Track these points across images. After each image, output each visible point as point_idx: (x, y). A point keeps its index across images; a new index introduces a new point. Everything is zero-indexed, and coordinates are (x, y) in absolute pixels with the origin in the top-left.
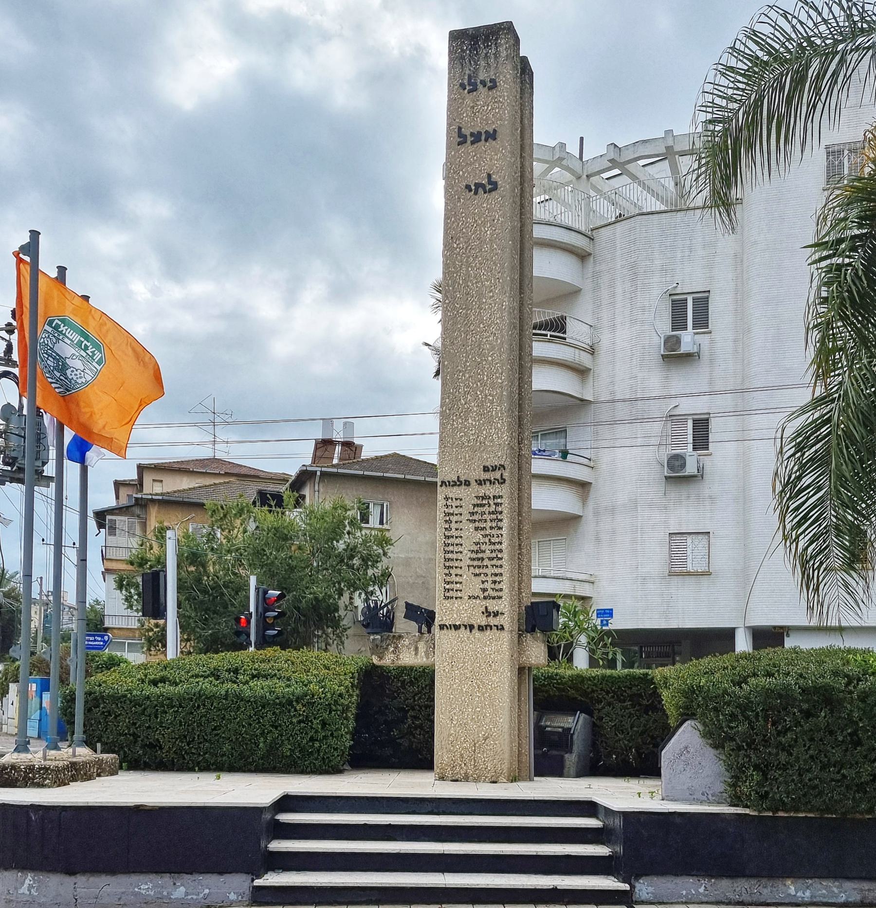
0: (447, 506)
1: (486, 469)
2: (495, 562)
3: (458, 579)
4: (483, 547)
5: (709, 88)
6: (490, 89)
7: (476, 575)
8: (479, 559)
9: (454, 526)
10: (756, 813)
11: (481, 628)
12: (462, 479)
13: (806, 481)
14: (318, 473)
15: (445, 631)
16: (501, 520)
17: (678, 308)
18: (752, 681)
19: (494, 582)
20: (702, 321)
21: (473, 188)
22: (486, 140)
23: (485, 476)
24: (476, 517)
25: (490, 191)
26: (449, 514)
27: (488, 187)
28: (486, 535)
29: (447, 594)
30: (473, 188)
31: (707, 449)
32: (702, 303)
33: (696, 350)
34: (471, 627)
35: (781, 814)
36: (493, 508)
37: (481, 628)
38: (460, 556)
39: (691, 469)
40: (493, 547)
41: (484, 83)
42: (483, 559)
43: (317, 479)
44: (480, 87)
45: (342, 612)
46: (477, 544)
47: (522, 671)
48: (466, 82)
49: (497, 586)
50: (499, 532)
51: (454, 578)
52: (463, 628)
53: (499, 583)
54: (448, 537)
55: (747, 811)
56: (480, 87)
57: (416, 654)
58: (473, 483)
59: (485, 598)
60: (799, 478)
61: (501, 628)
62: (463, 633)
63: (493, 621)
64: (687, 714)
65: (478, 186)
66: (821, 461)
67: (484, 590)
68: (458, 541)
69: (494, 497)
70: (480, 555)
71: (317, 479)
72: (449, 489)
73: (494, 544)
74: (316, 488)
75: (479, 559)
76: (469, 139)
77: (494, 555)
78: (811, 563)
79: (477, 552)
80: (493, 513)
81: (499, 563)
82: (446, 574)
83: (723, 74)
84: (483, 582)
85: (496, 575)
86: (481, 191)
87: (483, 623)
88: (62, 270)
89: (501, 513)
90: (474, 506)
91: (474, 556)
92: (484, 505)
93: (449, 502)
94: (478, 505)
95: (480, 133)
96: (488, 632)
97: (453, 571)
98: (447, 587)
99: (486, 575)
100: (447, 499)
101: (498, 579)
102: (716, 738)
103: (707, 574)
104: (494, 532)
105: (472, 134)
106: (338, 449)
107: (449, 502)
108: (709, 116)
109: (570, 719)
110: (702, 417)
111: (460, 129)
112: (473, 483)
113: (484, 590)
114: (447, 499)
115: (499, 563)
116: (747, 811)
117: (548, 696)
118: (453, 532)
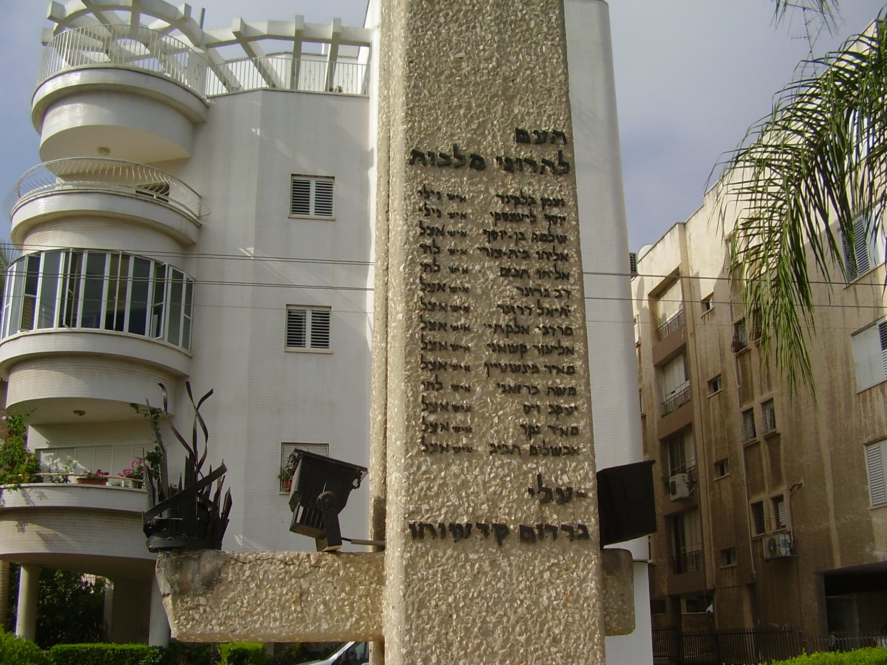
3: (457, 399)
4: (524, 320)
19: (557, 410)
46: (507, 309)
62: (478, 553)
67: (531, 431)
79: (508, 331)
97: (447, 377)
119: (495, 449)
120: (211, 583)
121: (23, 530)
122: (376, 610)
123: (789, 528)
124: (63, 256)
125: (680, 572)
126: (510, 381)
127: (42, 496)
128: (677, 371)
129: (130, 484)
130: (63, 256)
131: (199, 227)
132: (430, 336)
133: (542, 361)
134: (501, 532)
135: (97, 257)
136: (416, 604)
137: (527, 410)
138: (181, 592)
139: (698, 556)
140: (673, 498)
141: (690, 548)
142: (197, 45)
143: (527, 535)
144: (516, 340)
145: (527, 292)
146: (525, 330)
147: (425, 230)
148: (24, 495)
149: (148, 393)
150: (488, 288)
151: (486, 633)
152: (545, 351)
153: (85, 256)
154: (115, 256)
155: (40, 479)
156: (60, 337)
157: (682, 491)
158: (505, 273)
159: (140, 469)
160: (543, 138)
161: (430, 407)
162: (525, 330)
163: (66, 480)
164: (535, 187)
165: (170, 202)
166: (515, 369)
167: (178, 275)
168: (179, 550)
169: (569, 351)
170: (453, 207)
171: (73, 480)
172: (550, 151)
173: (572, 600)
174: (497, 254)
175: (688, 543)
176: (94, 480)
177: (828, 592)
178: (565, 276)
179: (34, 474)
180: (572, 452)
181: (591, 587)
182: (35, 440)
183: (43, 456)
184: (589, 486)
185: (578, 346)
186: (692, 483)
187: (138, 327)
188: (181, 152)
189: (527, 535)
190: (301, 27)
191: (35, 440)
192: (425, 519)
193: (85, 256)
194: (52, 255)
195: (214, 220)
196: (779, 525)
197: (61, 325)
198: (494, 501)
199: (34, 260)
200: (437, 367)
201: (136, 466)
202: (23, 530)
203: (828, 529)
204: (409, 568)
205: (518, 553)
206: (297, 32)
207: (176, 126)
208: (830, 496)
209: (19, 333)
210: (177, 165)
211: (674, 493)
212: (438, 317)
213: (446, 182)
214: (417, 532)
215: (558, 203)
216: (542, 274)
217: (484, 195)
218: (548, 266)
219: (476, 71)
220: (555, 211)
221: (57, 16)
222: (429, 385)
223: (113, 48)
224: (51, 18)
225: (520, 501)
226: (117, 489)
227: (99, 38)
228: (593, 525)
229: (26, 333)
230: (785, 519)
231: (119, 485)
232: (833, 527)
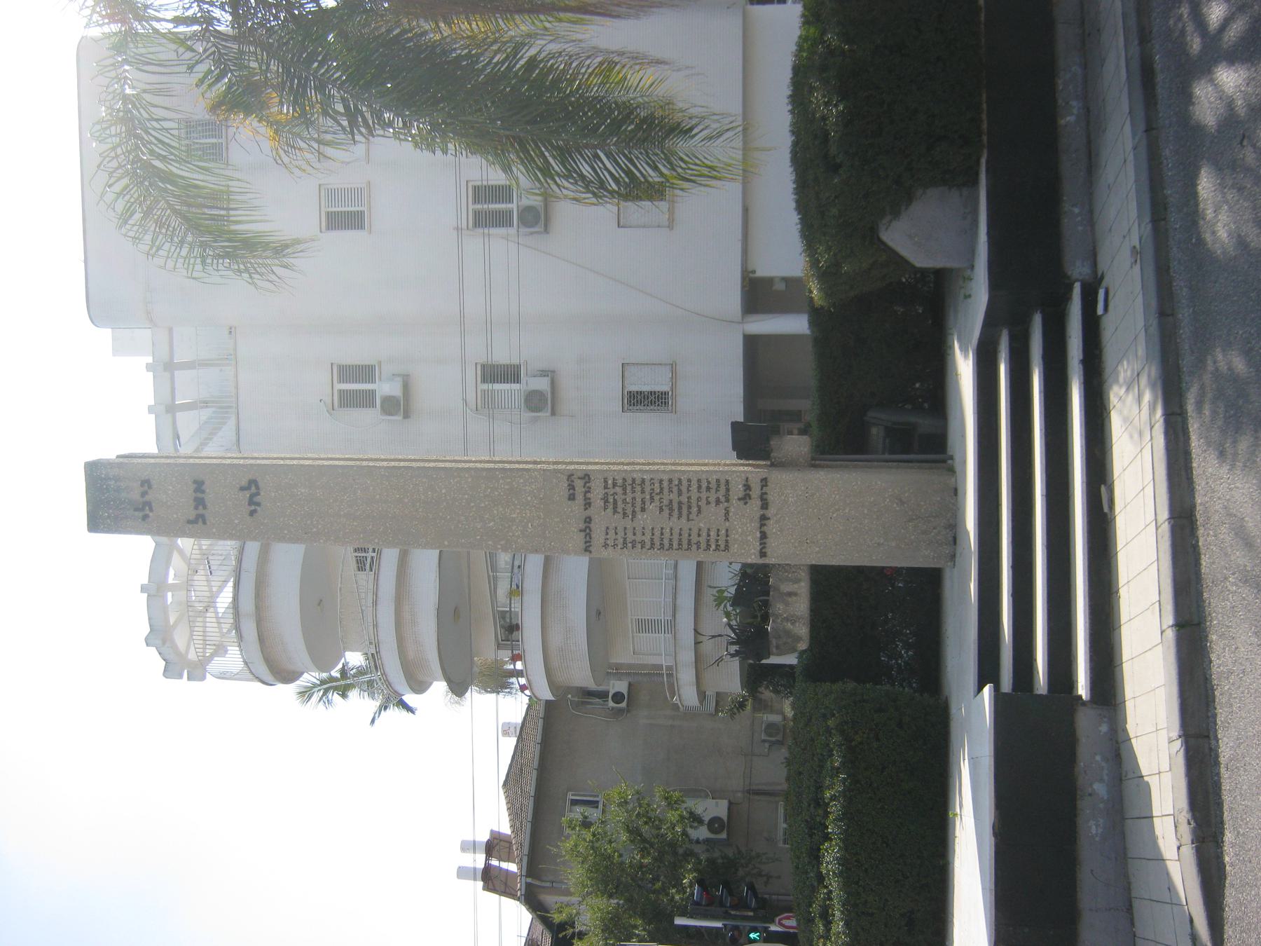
0: (615, 546)
1: (572, 498)
2: (684, 489)
3: (704, 534)
4: (666, 502)
5: (170, 264)
6: (150, 487)
7: (699, 511)
8: (680, 508)
9: (639, 538)
10: (985, 151)
11: (765, 506)
12: (582, 526)
13: (586, 170)
14: (529, 880)
15: (769, 551)
16: (634, 480)
17: (349, 400)
18: (833, 150)
19: (708, 489)
20: (366, 372)
21: (253, 508)
22: (203, 492)
23: (580, 498)
24: (629, 512)
25: (257, 488)
26: (625, 543)
27: (253, 489)
28: (652, 498)
29: (722, 547)
30: (253, 508)
31: (519, 367)
32: (348, 372)
33: (399, 379)
34: (764, 518)
35: (985, 126)
36: (618, 490)
37: (765, 506)
38: (676, 531)
39: (542, 384)
40: (666, 491)
41: (144, 494)
42: (680, 503)
43: (537, 883)
44: (147, 498)
45: (717, 854)
46: (661, 509)
47: (813, 464)
48: (141, 514)
49: (713, 485)
50: (647, 483)
51: (703, 540)
52: (765, 528)
53: (709, 483)
54: (653, 544)
55: (983, 161)
56: (147, 498)
57: (795, 594)
58: (588, 513)
59: (727, 501)
60: (582, 177)
61: (764, 482)
62: (771, 528)
63: (756, 492)
64: (871, 236)
65: (251, 502)
66: (564, 154)
67: (718, 502)
68: (657, 533)
69: (606, 487)
70: (675, 506)
71: (537, 883)
72: (594, 542)
73: (662, 489)
74: (548, 884)
75: (680, 508)
76: (201, 511)
77: (675, 489)
78: (679, 170)
79: (671, 510)
80: (625, 489)
81: (685, 483)
82: (698, 548)
83: (159, 249)
84: (708, 503)
85: (699, 487)
86: (257, 499)
87: (759, 503)
88: (409, 709)
89: (624, 480)
90: (615, 512)
91: (676, 513)
92: (615, 500)
93: (610, 542)
94: (615, 508)
95: (196, 499)
96: (770, 498)
97: (694, 539)
98: (713, 547)
99: (699, 499)
100: (606, 545)
101: (704, 485)
102: (899, 198)
103: (673, 367)
104: (648, 489)
105: (196, 508)
106: (494, 862)
107: (610, 542)
108: (199, 261)
109: (874, 430)
110: (479, 372)
111: (189, 522)
112: (588, 513)
113: (718, 502)
114: (606, 545)
115: (685, 483)
116: (983, 161)
117: (843, 440)
118: (647, 538)
119: (727, 519)
150: (649, 519)
164: (597, 493)
205: (771, 512)
213: (598, 536)
215: (606, 481)
216: (643, 492)
217: (602, 520)
228: (763, 473)
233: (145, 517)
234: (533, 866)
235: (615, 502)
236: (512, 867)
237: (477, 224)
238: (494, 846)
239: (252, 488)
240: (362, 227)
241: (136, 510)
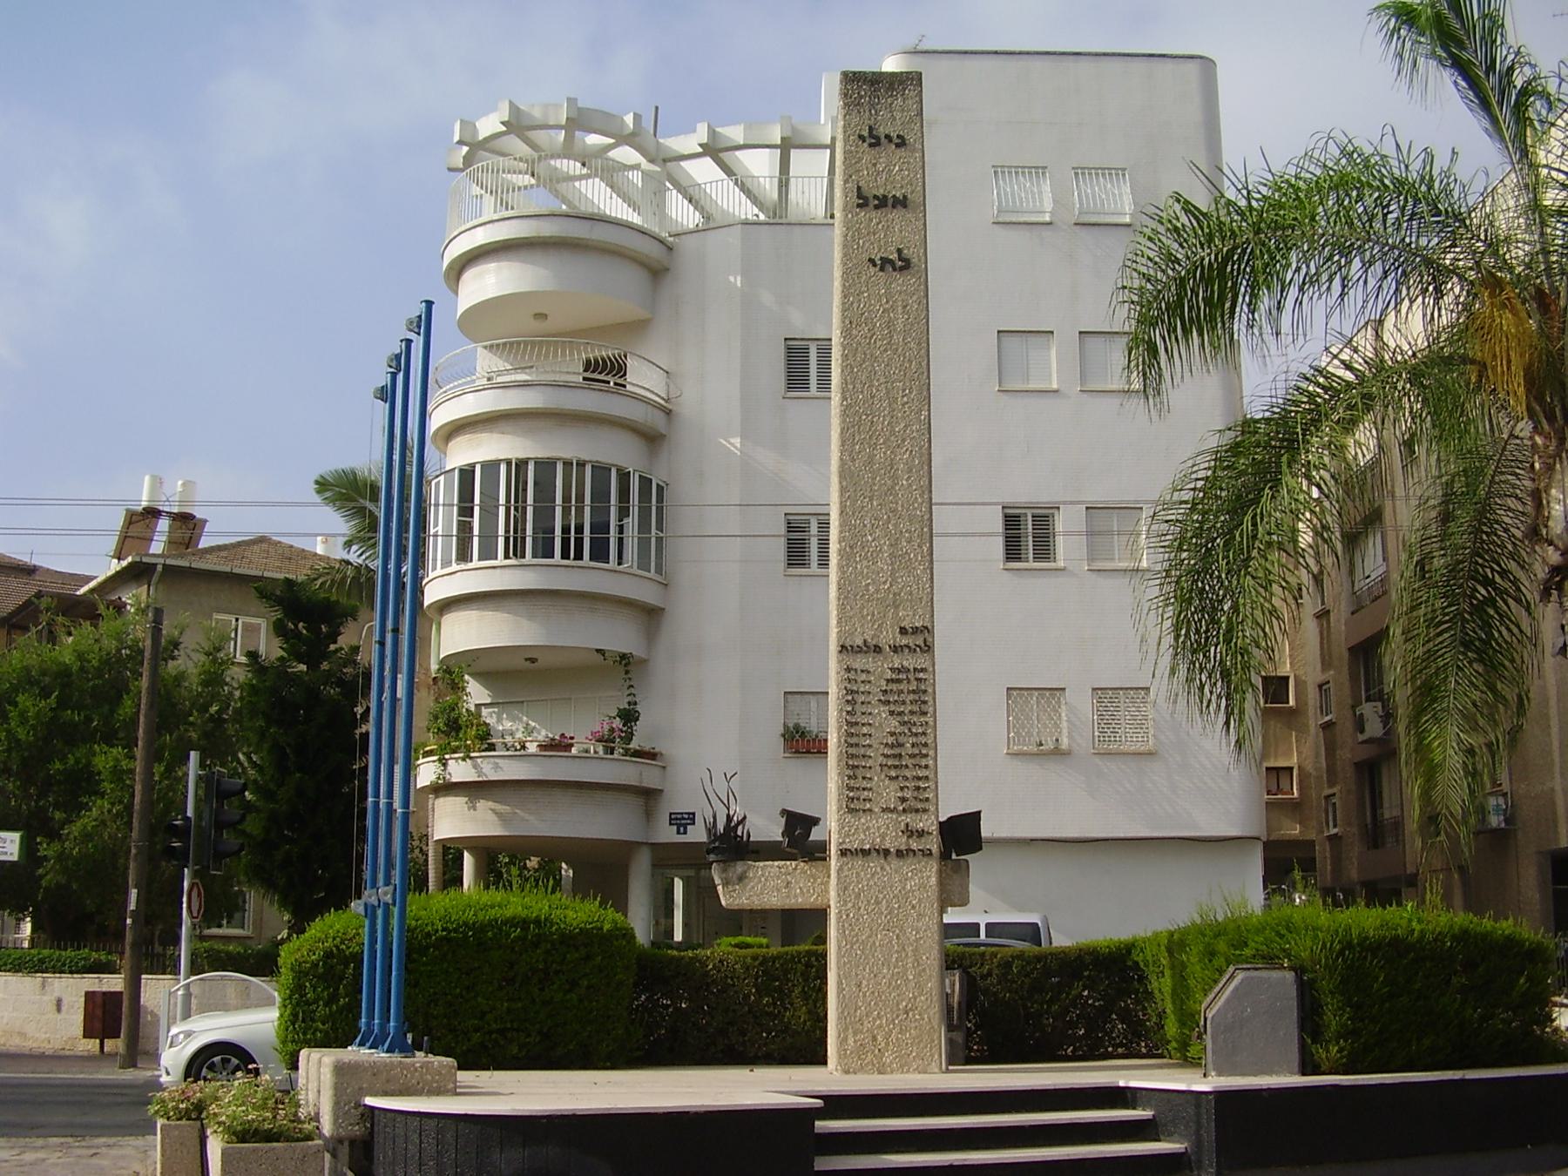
3: (865, 784)
4: (901, 739)
14: (159, 568)
19: (918, 788)
25: (901, 269)
46: (892, 734)
48: (866, 133)
62: (874, 864)
67: (903, 800)
79: (892, 746)
91: (888, 751)
97: (860, 773)
119: (884, 810)
120: (741, 878)
121: (475, 809)
122: (827, 892)
123: (1506, 787)
124: (503, 468)
125: (1376, 846)
126: (893, 774)
127: (497, 767)
128: (1372, 550)
129: (600, 749)
130: (503, 468)
131: (669, 413)
132: (851, 751)
133: (910, 762)
134: (887, 852)
135: (545, 467)
136: (843, 888)
137: (902, 789)
138: (726, 883)
139: (1398, 824)
140: (1361, 738)
141: (1388, 813)
142: (652, 161)
143: (900, 854)
144: (896, 751)
145: (904, 723)
146: (901, 745)
147: (849, 692)
148: (475, 766)
149: (619, 636)
150: (882, 722)
151: (878, 903)
152: (912, 756)
153: (531, 467)
154: (567, 464)
155: (492, 747)
156: (507, 571)
157: (1374, 728)
158: (892, 713)
159: (612, 730)
160: (916, 631)
161: (851, 789)
162: (901, 745)
163: (523, 747)
164: (909, 662)
165: (629, 387)
166: (896, 767)
167: (645, 483)
168: (724, 862)
169: (926, 756)
170: (863, 677)
171: (532, 748)
172: (920, 638)
173: (922, 887)
174: (888, 702)
175: (1386, 805)
176: (558, 746)
177: (1557, 879)
178: (925, 714)
179: (485, 740)
180: (925, 811)
181: (933, 880)
182: (476, 693)
183: (484, 712)
184: (934, 828)
185: (931, 753)
186: (1388, 717)
187: (600, 553)
188: (642, 314)
189: (900, 854)
190: (788, 134)
191: (476, 693)
192: (848, 846)
193: (531, 467)
194: (491, 467)
195: (687, 405)
196: (1495, 783)
197: (507, 557)
198: (883, 837)
199: (467, 474)
200: (854, 767)
201: (606, 728)
202: (475, 809)
203: (1553, 790)
204: (840, 870)
205: (895, 862)
206: (783, 139)
207: (630, 279)
208: (1556, 744)
209: (455, 567)
210: (637, 328)
211: (1362, 731)
212: (854, 740)
213: (859, 662)
214: (844, 853)
215: (922, 670)
216: (912, 713)
217: (880, 667)
218: (916, 708)
219: (877, 591)
220: (921, 675)
221: (468, 139)
222: (849, 777)
223: (541, 169)
224: (461, 142)
225: (897, 836)
226: (585, 756)
227: (521, 160)
228: (935, 849)
229: (463, 566)
230: (1503, 777)
231: (587, 751)
232: (1558, 788)
233: (861, 137)
234: (174, 575)
235: (899, 681)
236: (157, 547)
237: (791, 527)
238: (187, 524)
239: (901, 264)
240: (789, 388)
241: (871, 128)
